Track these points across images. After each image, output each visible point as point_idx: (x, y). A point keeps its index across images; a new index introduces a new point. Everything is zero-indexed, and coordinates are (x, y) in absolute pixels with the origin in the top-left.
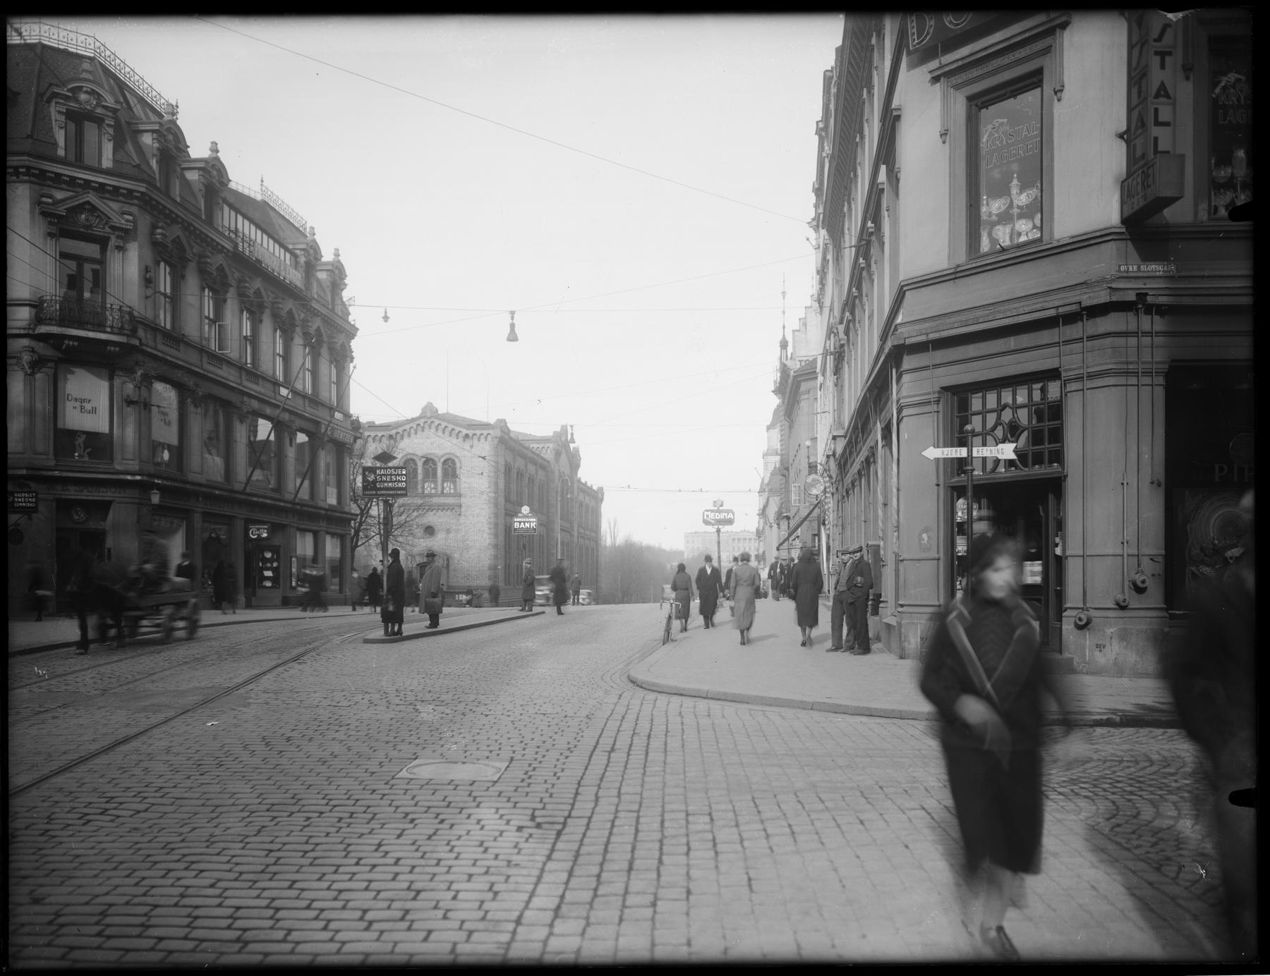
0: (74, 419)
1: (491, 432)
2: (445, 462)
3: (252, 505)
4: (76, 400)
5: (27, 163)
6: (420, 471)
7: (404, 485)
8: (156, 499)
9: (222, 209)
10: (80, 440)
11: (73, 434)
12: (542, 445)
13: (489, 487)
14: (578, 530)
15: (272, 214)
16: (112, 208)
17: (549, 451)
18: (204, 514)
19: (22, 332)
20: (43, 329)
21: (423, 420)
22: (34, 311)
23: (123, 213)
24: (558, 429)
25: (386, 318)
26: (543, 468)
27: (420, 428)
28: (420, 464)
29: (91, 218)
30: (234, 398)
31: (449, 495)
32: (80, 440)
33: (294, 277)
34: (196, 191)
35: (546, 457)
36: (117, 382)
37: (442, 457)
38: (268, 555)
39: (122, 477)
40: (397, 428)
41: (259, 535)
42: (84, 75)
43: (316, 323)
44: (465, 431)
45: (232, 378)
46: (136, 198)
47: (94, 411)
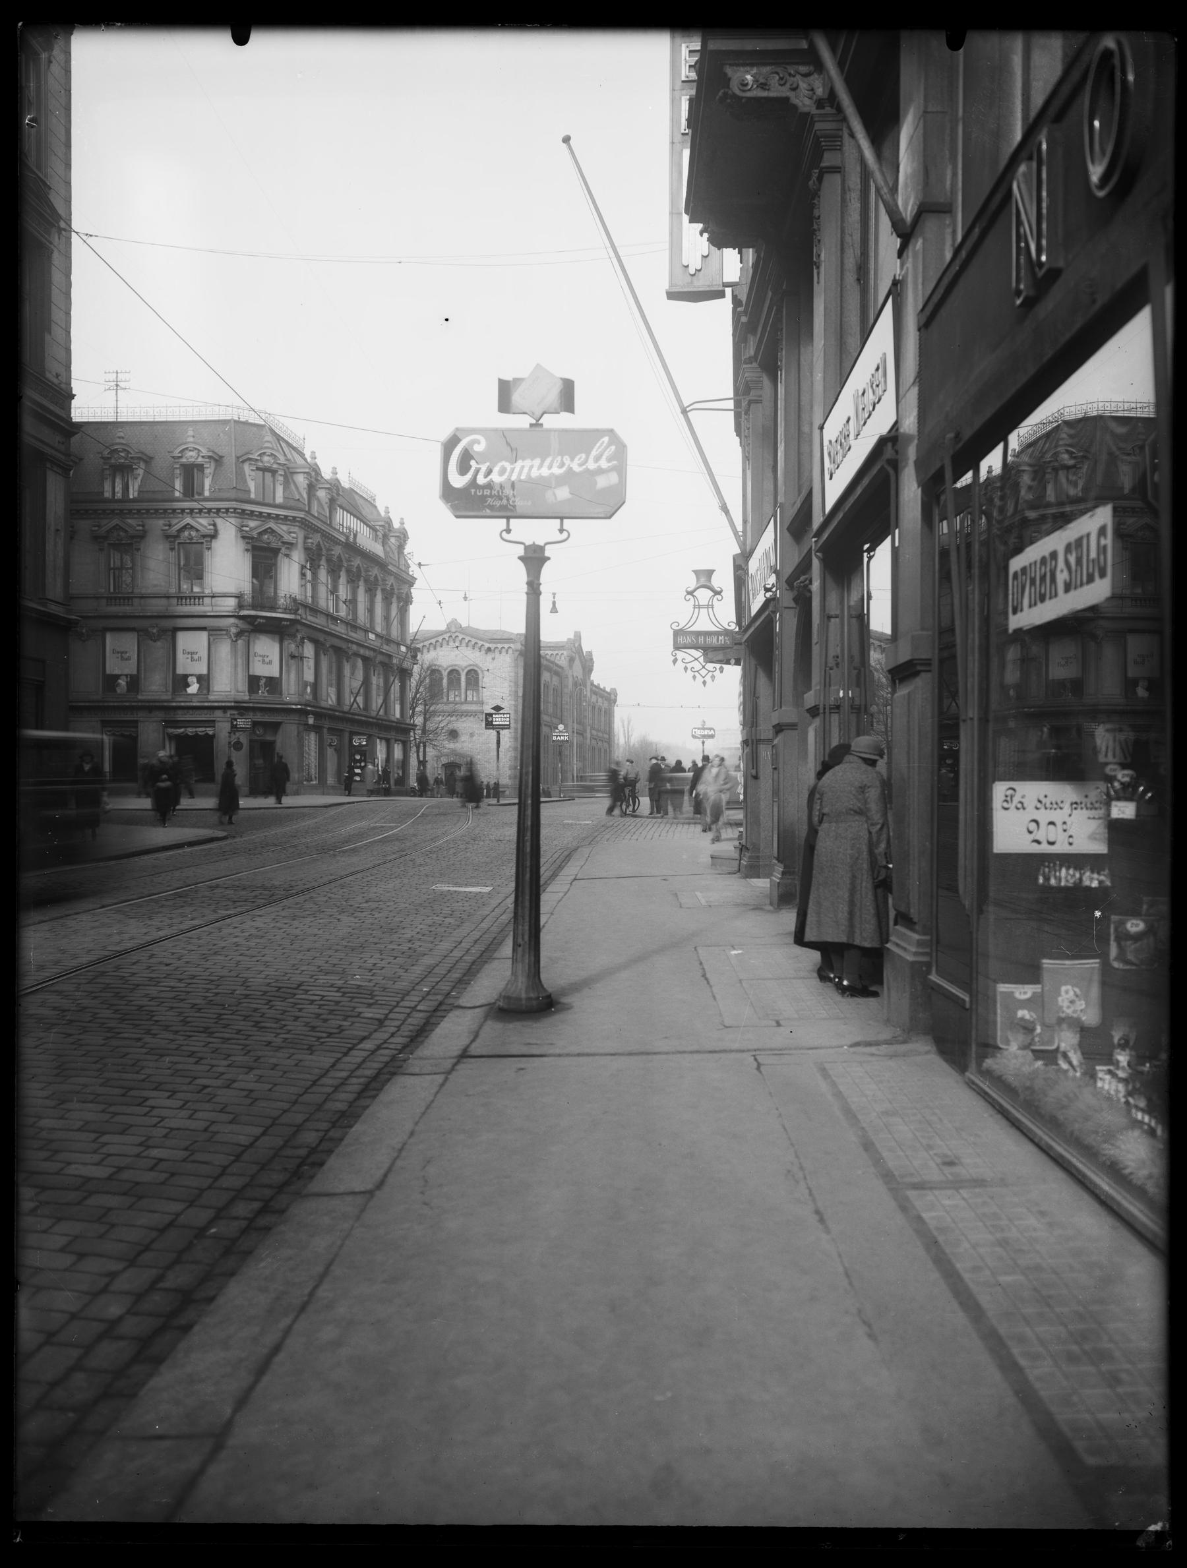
0: (259, 669)
1: (512, 645)
2: (469, 672)
3: (353, 721)
4: (260, 656)
5: (235, 506)
6: (445, 681)
7: (508, 723)
8: (311, 721)
9: (336, 509)
10: (262, 682)
11: (258, 678)
12: (556, 652)
13: (510, 695)
14: (591, 732)
15: (357, 497)
16: (282, 529)
17: (563, 658)
18: (329, 729)
19: (231, 614)
20: (243, 613)
21: (448, 635)
22: (237, 600)
23: (290, 533)
24: (572, 637)
25: (465, 598)
26: (557, 674)
27: (445, 642)
28: (445, 674)
29: (271, 537)
30: (343, 645)
31: (472, 703)
32: (262, 682)
33: (377, 549)
34: (324, 503)
35: (560, 663)
36: (285, 643)
37: (466, 667)
38: (358, 757)
39: (289, 706)
40: (423, 642)
41: (360, 743)
42: (267, 445)
43: (391, 581)
44: (487, 645)
45: (343, 631)
46: (298, 521)
47: (270, 662)
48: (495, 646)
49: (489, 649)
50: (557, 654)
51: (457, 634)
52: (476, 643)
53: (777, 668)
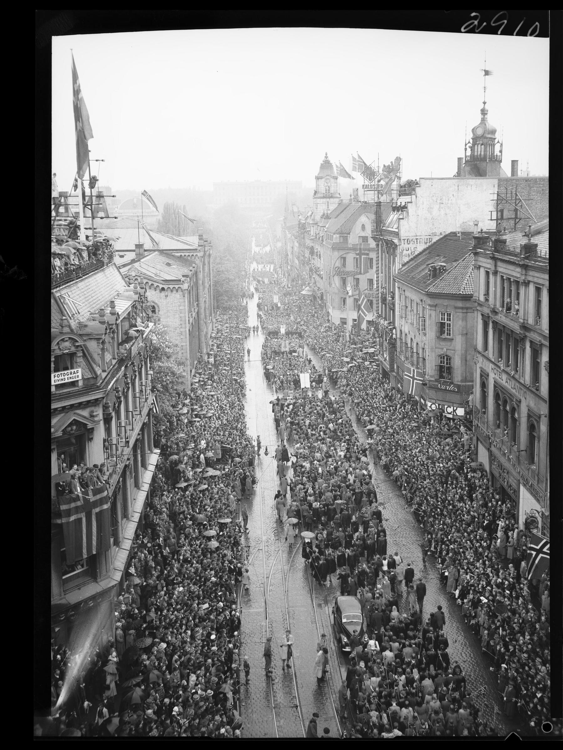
12: (192, 254)
44: (161, 286)
48: (168, 286)
49: (163, 289)
50: (193, 255)
51: (136, 277)
52: (152, 284)
53: (66, 313)
